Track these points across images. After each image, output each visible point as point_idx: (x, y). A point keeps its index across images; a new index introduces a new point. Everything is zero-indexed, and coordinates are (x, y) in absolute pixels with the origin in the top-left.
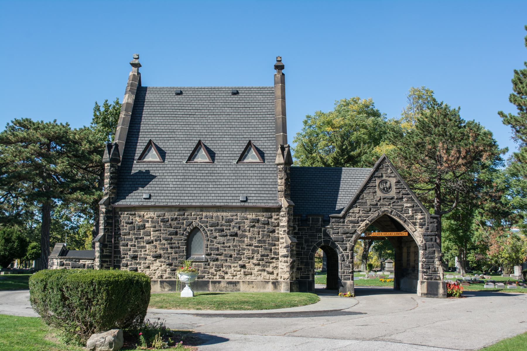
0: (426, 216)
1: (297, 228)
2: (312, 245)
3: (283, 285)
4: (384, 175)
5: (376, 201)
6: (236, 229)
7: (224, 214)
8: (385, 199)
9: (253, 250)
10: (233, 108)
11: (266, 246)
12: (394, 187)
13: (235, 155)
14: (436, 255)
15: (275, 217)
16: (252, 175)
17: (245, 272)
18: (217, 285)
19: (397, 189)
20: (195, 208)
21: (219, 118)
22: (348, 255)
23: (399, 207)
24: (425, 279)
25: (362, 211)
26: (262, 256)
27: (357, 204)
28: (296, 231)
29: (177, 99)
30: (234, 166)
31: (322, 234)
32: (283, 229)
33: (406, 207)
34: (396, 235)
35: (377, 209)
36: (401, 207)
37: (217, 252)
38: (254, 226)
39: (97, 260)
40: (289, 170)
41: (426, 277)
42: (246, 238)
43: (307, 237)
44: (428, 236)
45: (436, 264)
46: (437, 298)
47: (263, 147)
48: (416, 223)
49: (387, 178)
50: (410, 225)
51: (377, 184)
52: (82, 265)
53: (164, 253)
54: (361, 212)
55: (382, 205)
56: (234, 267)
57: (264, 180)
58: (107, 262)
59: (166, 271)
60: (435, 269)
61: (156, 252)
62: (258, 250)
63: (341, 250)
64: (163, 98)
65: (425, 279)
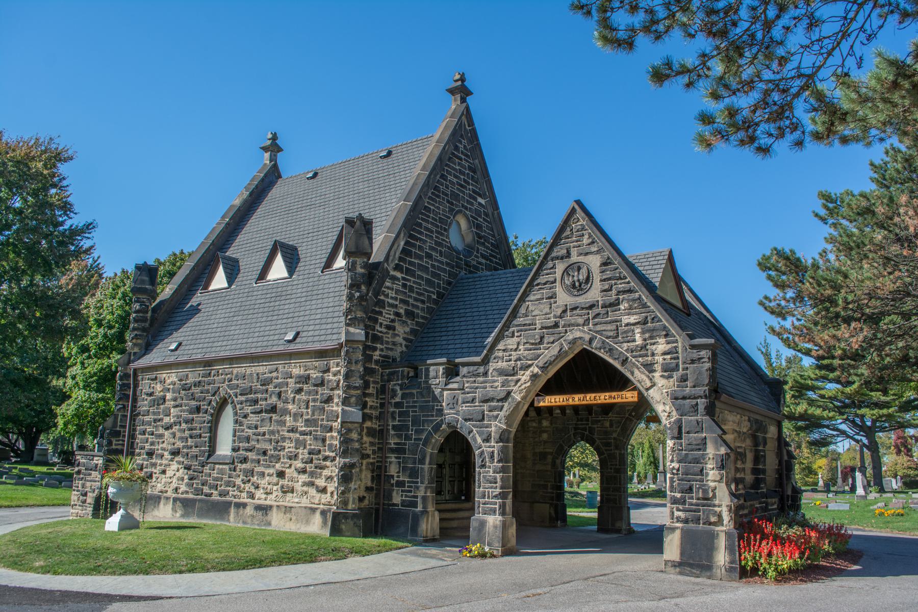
0: (680, 345)
1: (399, 392)
2: (423, 430)
4: (574, 252)
5: (555, 317)
6: (274, 400)
7: (261, 369)
8: (575, 308)
9: (297, 441)
11: (317, 431)
12: (597, 277)
14: (710, 451)
15: (334, 369)
17: (282, 487)
19: (604, 280)
20: (223, 361)
22: (493, 452)
23: (609, 327)
24: (679, 519)
25: (525, 344)
26: (310, 453)
27: (515, 329)
33: (627, 325)
34: (608, 401)
35: (557, 336)
36: (614, 327)
37: (247, 445)
38: (299, 391)
40: (361, 268)
41: (680, 513)
42: (288, 416)
44: (684, 398)
45: (709, 478)
48: (652, 364)
49: (581, 259)
50: (636, 372)
51: (558, 275)
53: (184, 447)
54: (521, 347)
55: (569, 326)
60: (705, 491)
61: (174, 444)
62: (304, 440)
63: (479, 440)
65: (679, 519)
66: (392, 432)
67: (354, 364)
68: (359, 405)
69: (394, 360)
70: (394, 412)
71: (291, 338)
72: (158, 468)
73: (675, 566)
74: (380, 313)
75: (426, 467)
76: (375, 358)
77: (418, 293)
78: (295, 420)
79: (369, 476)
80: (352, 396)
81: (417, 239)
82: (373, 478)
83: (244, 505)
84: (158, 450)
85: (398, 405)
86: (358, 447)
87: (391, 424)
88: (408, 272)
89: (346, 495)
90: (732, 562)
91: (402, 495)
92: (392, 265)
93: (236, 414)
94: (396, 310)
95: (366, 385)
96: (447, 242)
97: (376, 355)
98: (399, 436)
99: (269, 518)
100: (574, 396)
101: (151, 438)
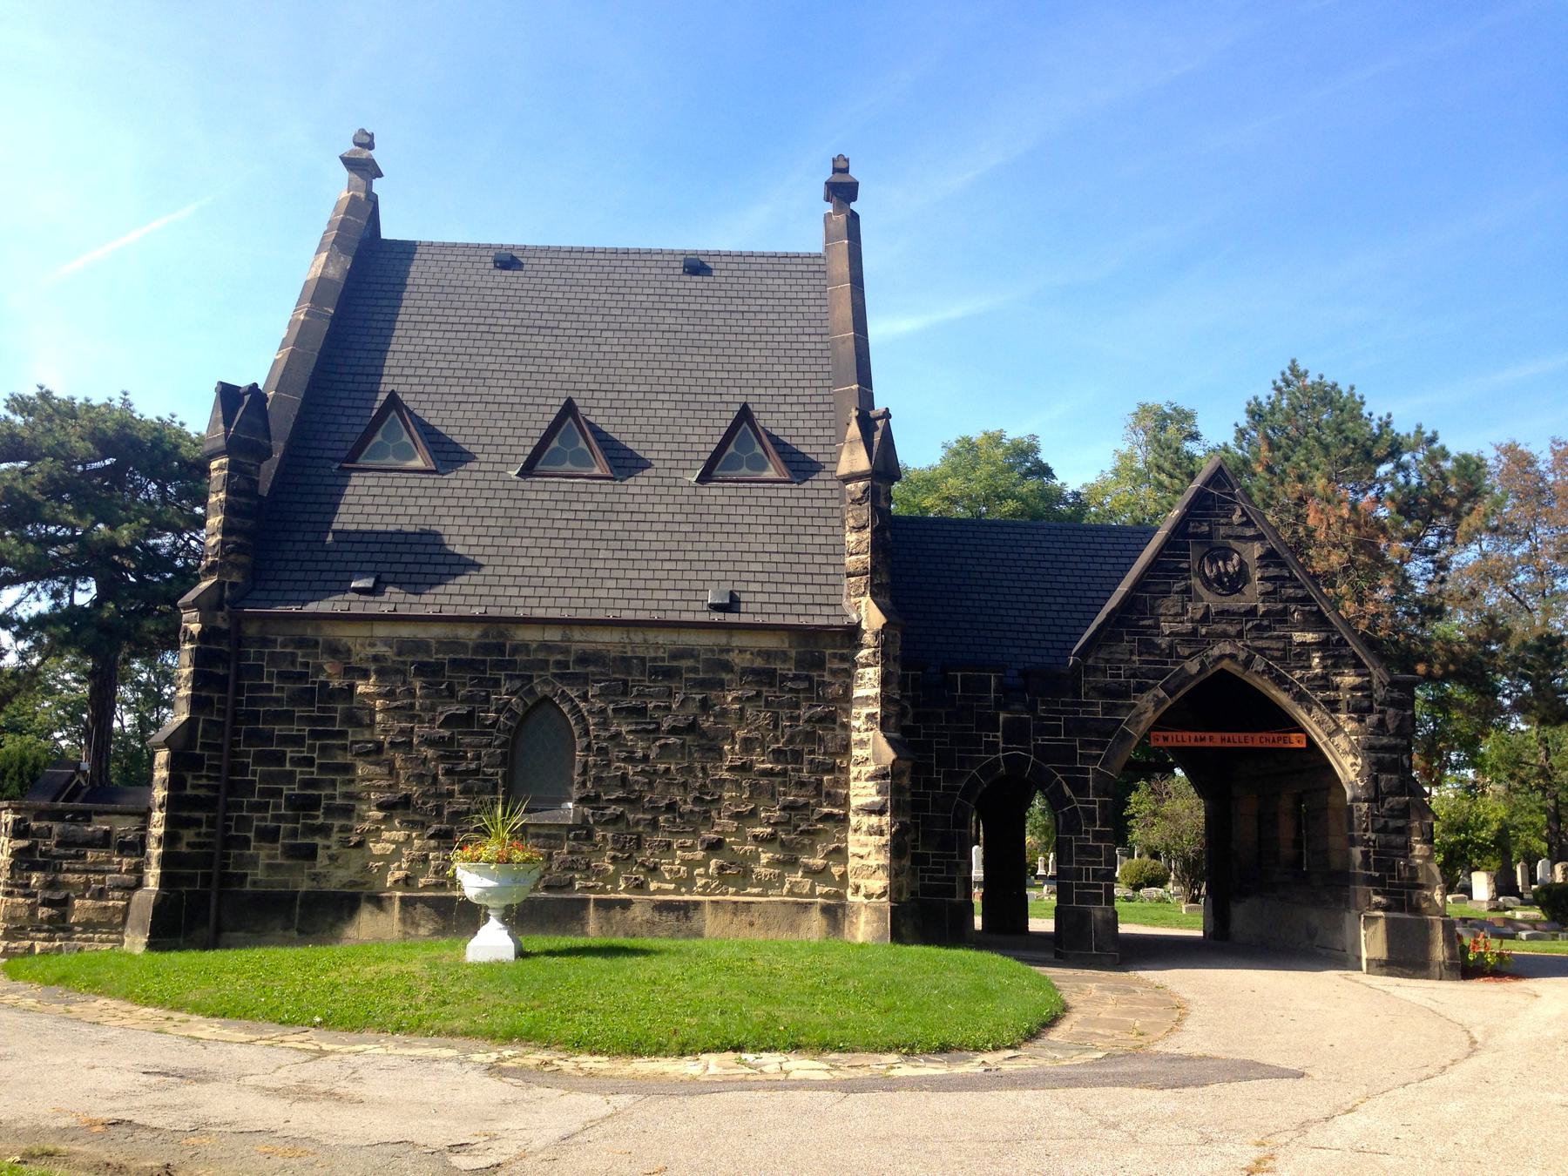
3: (863, 918)
10: (686, 314)
13: (694, 456)
16: (752, 520)
18: (617, 914)
21: (639, 341)
23: (1275, 645)
28: (907, 722)
29: (497, 279)
30: (686, 491)
31: (999, 734)
32: (866, 711)
33: (1300, 644)
39: (158, 816)
43: (945, 743)
45: (1416, 853)
46: (1427, 978)
47: (789, 432)
48: (1336, 702)
56: (682, 847)
57: (794, 539)
58: (198, 823)
59: (425, 859)
64: (449, 277)
73: (1381, 966)
84: (333, 797)
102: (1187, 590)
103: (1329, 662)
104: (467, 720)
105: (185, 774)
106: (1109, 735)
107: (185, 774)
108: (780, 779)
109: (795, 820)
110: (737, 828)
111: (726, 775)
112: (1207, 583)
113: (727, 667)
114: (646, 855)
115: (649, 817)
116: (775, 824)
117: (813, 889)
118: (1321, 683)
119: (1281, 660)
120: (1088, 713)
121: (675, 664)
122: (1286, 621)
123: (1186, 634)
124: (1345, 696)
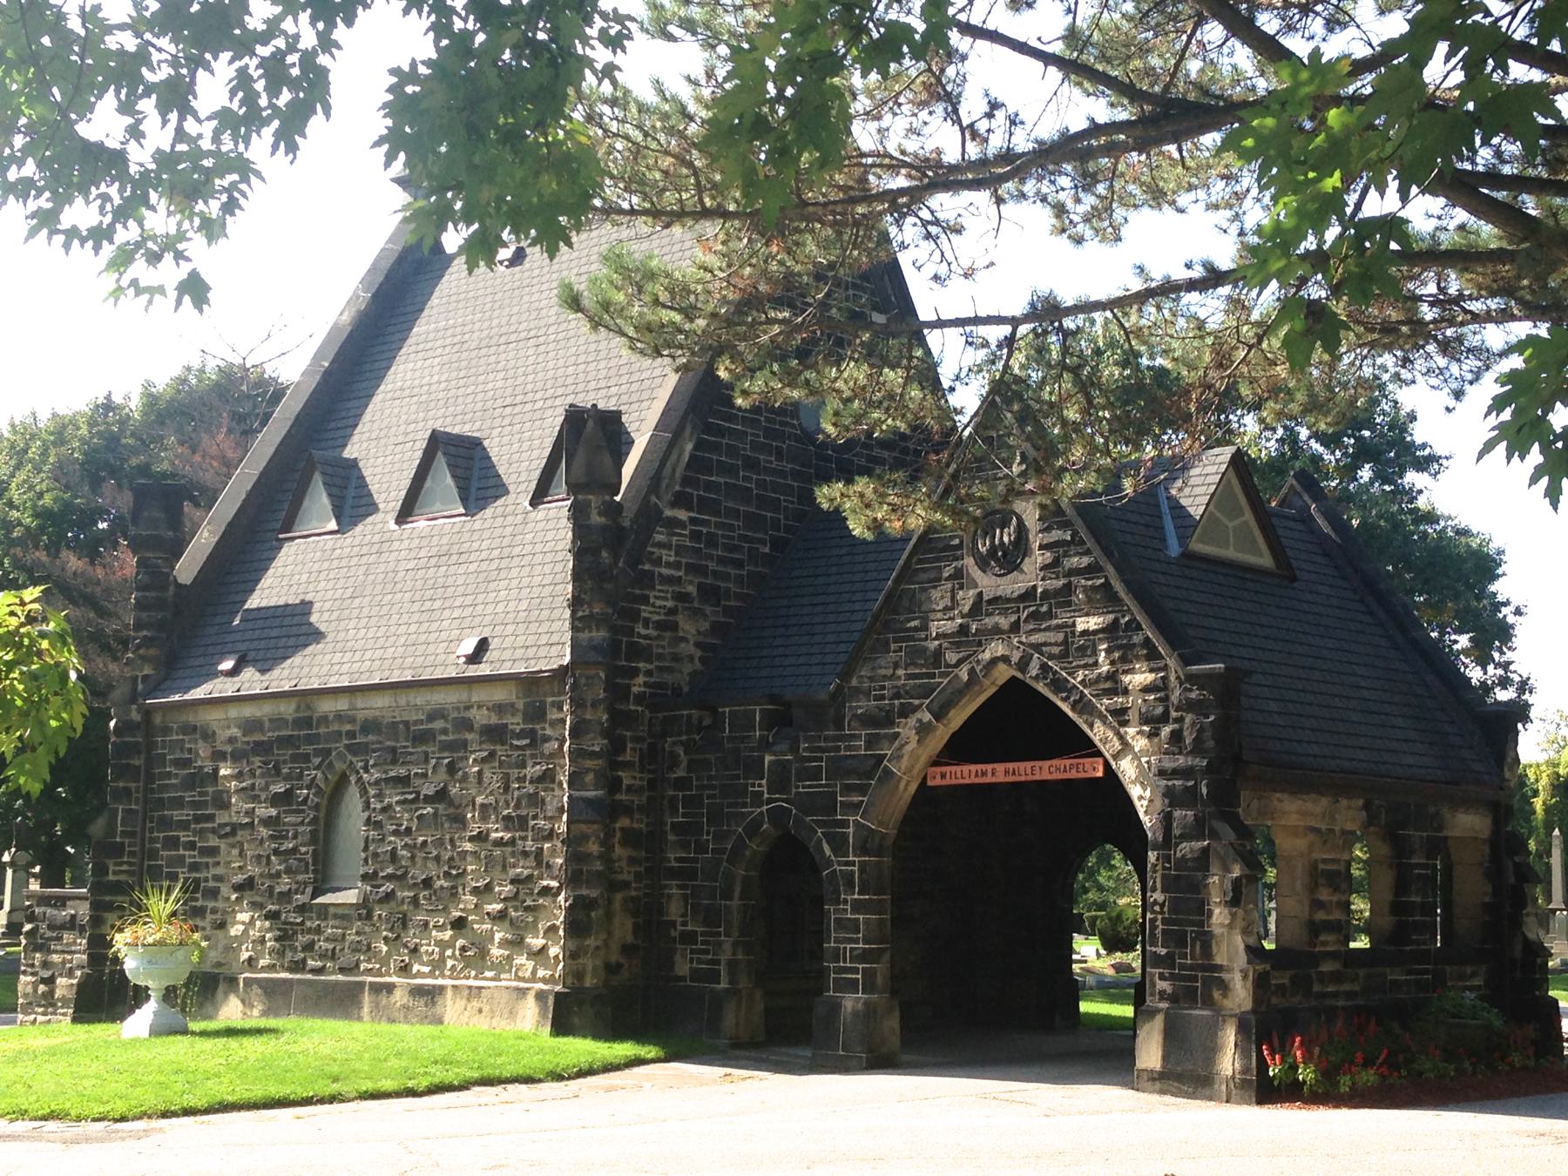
12: (1036, 540)
31: (764, 782)
33: (1085, 633)
36: (1060, 637)
40: (600, 514)
46: (1210, 1099)
52: (68, 918)
66: (671, 837)
67: (589, 709)
68: (602, 788)
69: (677, 691)
70: (675, 797)
71: (470, 651)
72: (209, 917)
73: (1153, 1079)
74: (645, 600)
75: (735, 903)
76: (635, 689)
77: (726, 547)
78: (484, 818)
79: (629, 924)
80: (588, 770)
81: (721, 432)
82: (636, 929)
83: (390, 988)
84: (206, 880)
85: (682, 784)
86: (601, 868)
87: (669, 821)
88: (704, 505)
89: (580, 961)
90: (1245, 1071)
91: (692, 960)
92: (668, 497)
93: (367, 806)
94: (677, 589)
95: (617, 745)
96: (793, 426)
97: (638, 685)
98: (685, 846)
99: (438, 1010)
100: (995, 765)
101: (190, 856)
102: (958, 574)
103: (1117, 655)
104: (287, 797)
105: (107, 861)
106: (870, 776)
107: (107, 861)
108: (510, 849)
109: (521, 896)
110: (476, 906)
111: (468, 846)
112: (983, 564)
113: (466, 725)
114: (411, 938)
115: (412, 894)
116: (505, 899)
117: (534, 972)
118: (1108, 685)
119: (1064, 656)
120: (848, 748)
121: (430, 726)
122: (1069, 604)
123: (952, 635)
124: (1134, 701)
